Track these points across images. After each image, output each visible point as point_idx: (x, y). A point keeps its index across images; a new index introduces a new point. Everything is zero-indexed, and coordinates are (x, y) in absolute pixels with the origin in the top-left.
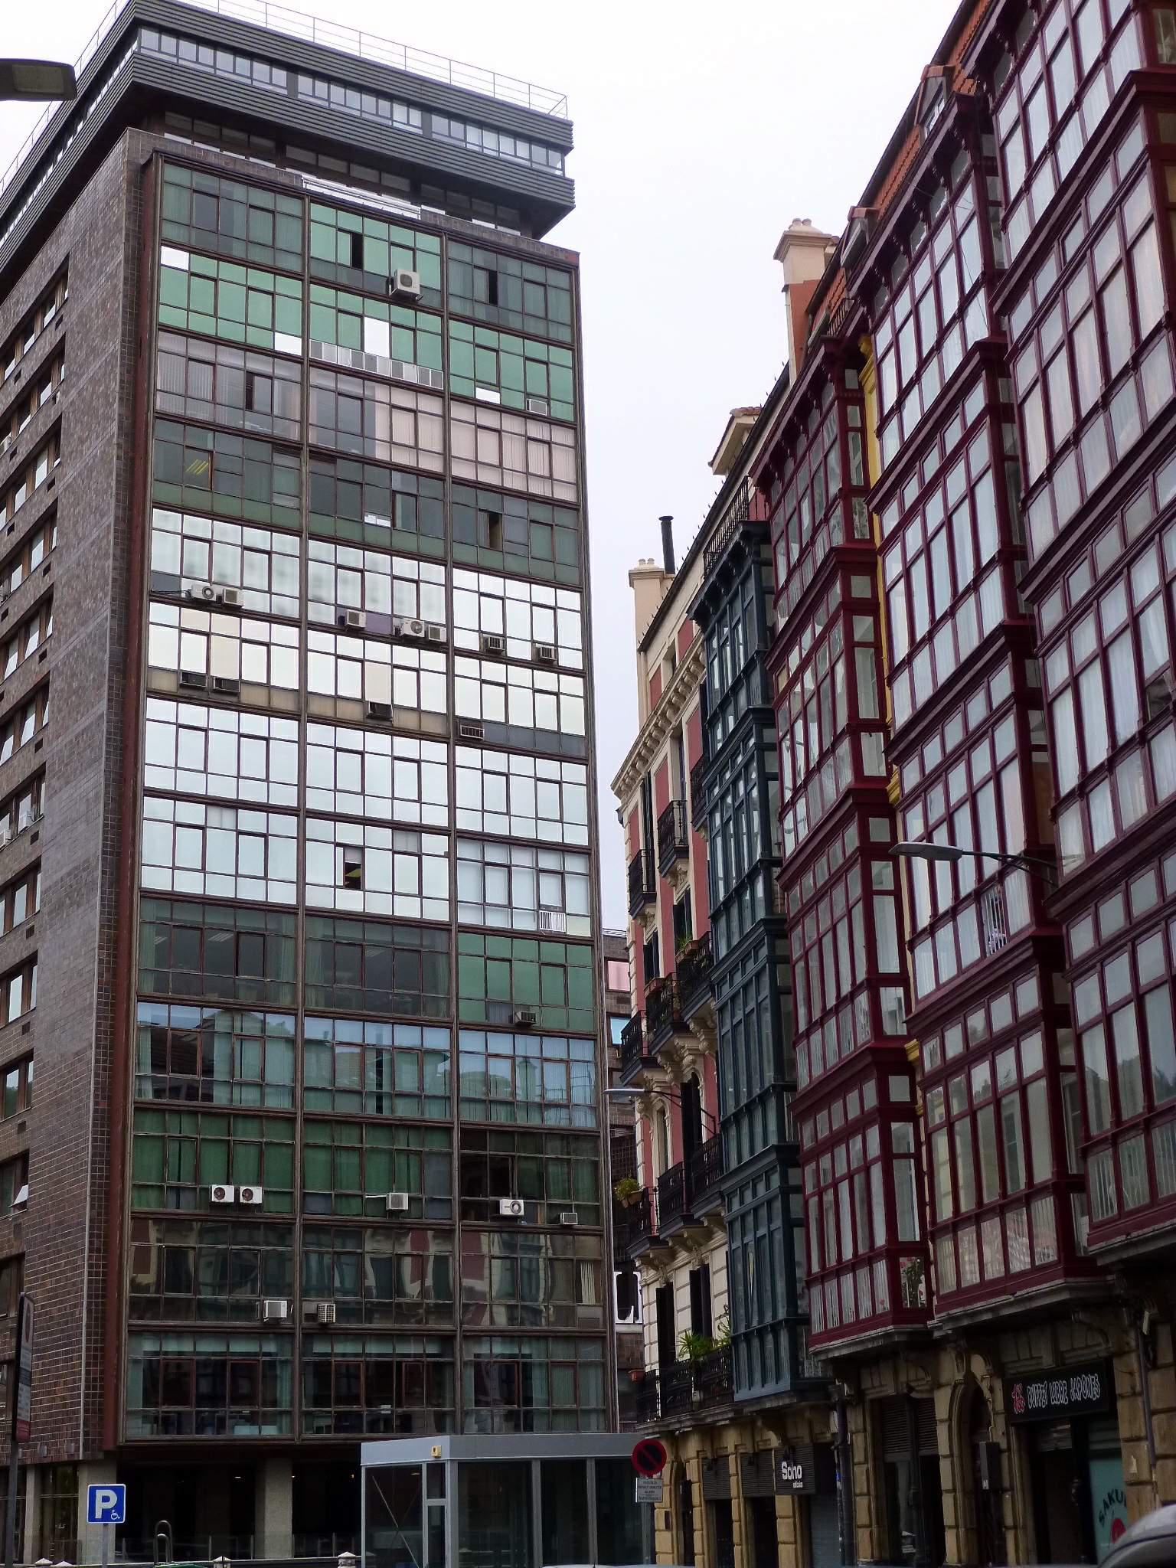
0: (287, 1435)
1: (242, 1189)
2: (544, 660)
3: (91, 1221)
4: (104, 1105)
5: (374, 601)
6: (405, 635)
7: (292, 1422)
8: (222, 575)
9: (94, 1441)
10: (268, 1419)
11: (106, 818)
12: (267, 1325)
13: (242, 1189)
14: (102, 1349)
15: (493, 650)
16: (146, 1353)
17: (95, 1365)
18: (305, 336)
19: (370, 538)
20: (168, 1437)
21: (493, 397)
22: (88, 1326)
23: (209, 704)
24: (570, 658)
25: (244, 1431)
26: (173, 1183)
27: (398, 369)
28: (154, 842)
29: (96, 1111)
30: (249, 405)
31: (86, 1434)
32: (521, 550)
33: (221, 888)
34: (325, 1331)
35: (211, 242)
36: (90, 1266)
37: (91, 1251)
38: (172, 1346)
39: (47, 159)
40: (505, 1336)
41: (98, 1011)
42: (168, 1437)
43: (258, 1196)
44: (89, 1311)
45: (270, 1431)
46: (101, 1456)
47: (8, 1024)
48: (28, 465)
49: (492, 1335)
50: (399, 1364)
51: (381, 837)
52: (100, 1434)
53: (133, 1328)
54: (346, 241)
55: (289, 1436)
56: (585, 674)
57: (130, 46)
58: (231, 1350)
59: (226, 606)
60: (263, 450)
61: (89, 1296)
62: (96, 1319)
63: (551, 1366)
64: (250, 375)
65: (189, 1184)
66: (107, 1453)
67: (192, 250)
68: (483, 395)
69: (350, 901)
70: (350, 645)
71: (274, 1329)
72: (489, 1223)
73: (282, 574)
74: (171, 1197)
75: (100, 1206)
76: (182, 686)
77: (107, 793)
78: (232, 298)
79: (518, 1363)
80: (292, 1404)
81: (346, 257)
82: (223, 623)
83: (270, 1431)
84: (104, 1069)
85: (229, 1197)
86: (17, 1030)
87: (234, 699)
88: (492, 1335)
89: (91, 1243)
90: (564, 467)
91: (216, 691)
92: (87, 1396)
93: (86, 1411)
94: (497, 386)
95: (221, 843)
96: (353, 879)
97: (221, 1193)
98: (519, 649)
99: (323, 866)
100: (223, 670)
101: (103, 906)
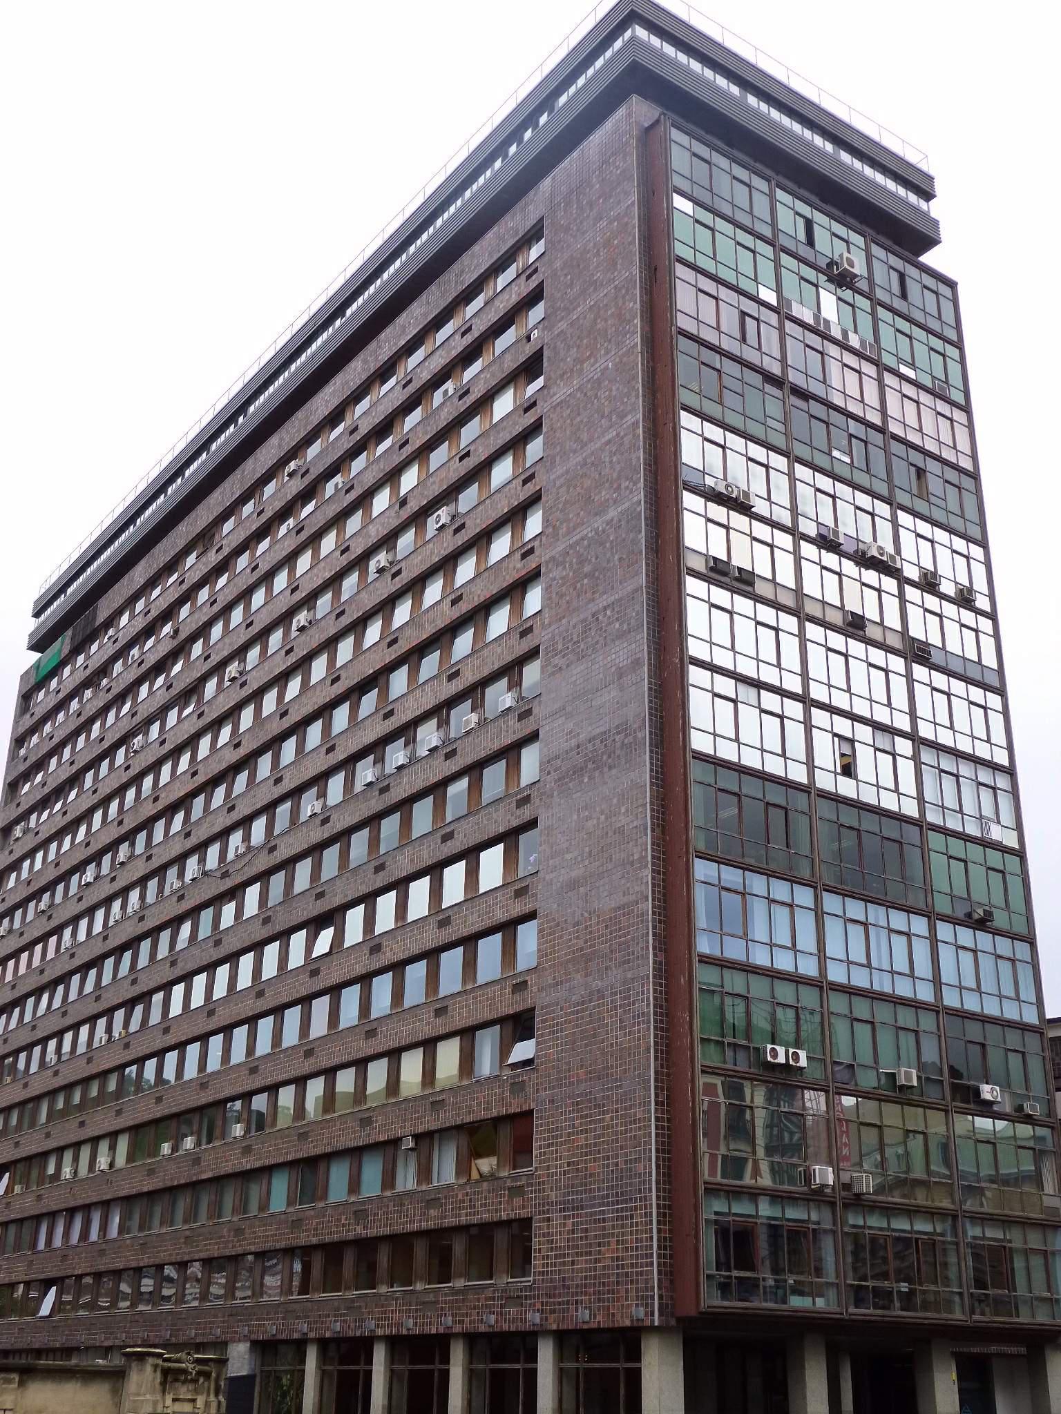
0: (834, 1308)
1: (791, 1051)
2: (965, 599)
3: (656, 1073)
4: (661, 958)
5: (844, 524)
6: (873, 557)
7: (839, 1294)
8: (734, 478)
9: (667, 1305)
10: (816, 1292)
11: (650, 683)
12: (814, 1192)
13: (791, 1051)
14: (670, 1207)
15: (929, 583)
16: (716, 1213)
17: (665, 1225)
18: (778, 290)
19: (838, 469)
20: (726, 1303)
21: (910, 373)
22: (658, 1182)
23: (733, 591)
24: (982, 603)
25: (796, 1302)
26: (731, 1040)
27: (845, 333)
28: (700, 707)
29: (655, 962)
30: (744, 339)
31: (660, 1297)
32: (942, 504)
33: (751, 759)
34: (857, 1202)
35: (706, 197)
36: (657, 1119)
37: (657, 1103)
38: (990, 1233)
39: (162, 489)
40: (776, 1197)
41: (653, 864)
42: (726, 1303)
43: (803, 1062)
44: (658, 1167)
45: (820, 1303)
46: (673, 1322)
47: (4, 985)
48: (316, 538)
49: (754, 1194)
50: (917, 1240)
51: (864, 733)
52: (672, 1298)
53: (709, 1186)
54: (801, 223)
55: (838, 1310)
56: (992, 616)
57: (484, 172)
58: (787, 1216)
59: (740, 505)
60: (756, 379)
61: (657, 1151)
62: (664, 1174)
63: (1027, 1253)
64: (743, 314)
65: (744, 1042)
66: (679, 1320)
67: (696, 202)
68: (904, 370)
69: (846, 788)
70: (831, 559)
71: (817, 1196)
72: (972, 1106)
73: (777, 487)
74: (729, 1053)
75: (662, 1059)
76: (712, 569)
77: (649, 659)
78: (725, 247)
79: (1005, 1247)
80: (837, 1276)
81: (802, 236)
82: (739, 520)
83: (820, 1303)
84: (660, 922)
85: (781, 1059)
86: (9, 987)
87: (749, 589)
88: (754, 1194)
89: (657, 1095)
90: (963, 444)
91: (737, 579)
92: (659, 1256)
93: (660, 1273)
94: (912, 365)
95: (748, 715)
96: (848, 770)
97: (775, 1055)
98: (947, 588)
99: (826, 752)
100: (740, 560)
101: (651, 764)
